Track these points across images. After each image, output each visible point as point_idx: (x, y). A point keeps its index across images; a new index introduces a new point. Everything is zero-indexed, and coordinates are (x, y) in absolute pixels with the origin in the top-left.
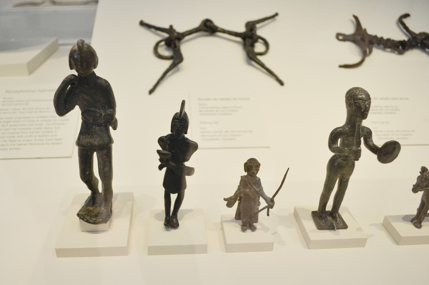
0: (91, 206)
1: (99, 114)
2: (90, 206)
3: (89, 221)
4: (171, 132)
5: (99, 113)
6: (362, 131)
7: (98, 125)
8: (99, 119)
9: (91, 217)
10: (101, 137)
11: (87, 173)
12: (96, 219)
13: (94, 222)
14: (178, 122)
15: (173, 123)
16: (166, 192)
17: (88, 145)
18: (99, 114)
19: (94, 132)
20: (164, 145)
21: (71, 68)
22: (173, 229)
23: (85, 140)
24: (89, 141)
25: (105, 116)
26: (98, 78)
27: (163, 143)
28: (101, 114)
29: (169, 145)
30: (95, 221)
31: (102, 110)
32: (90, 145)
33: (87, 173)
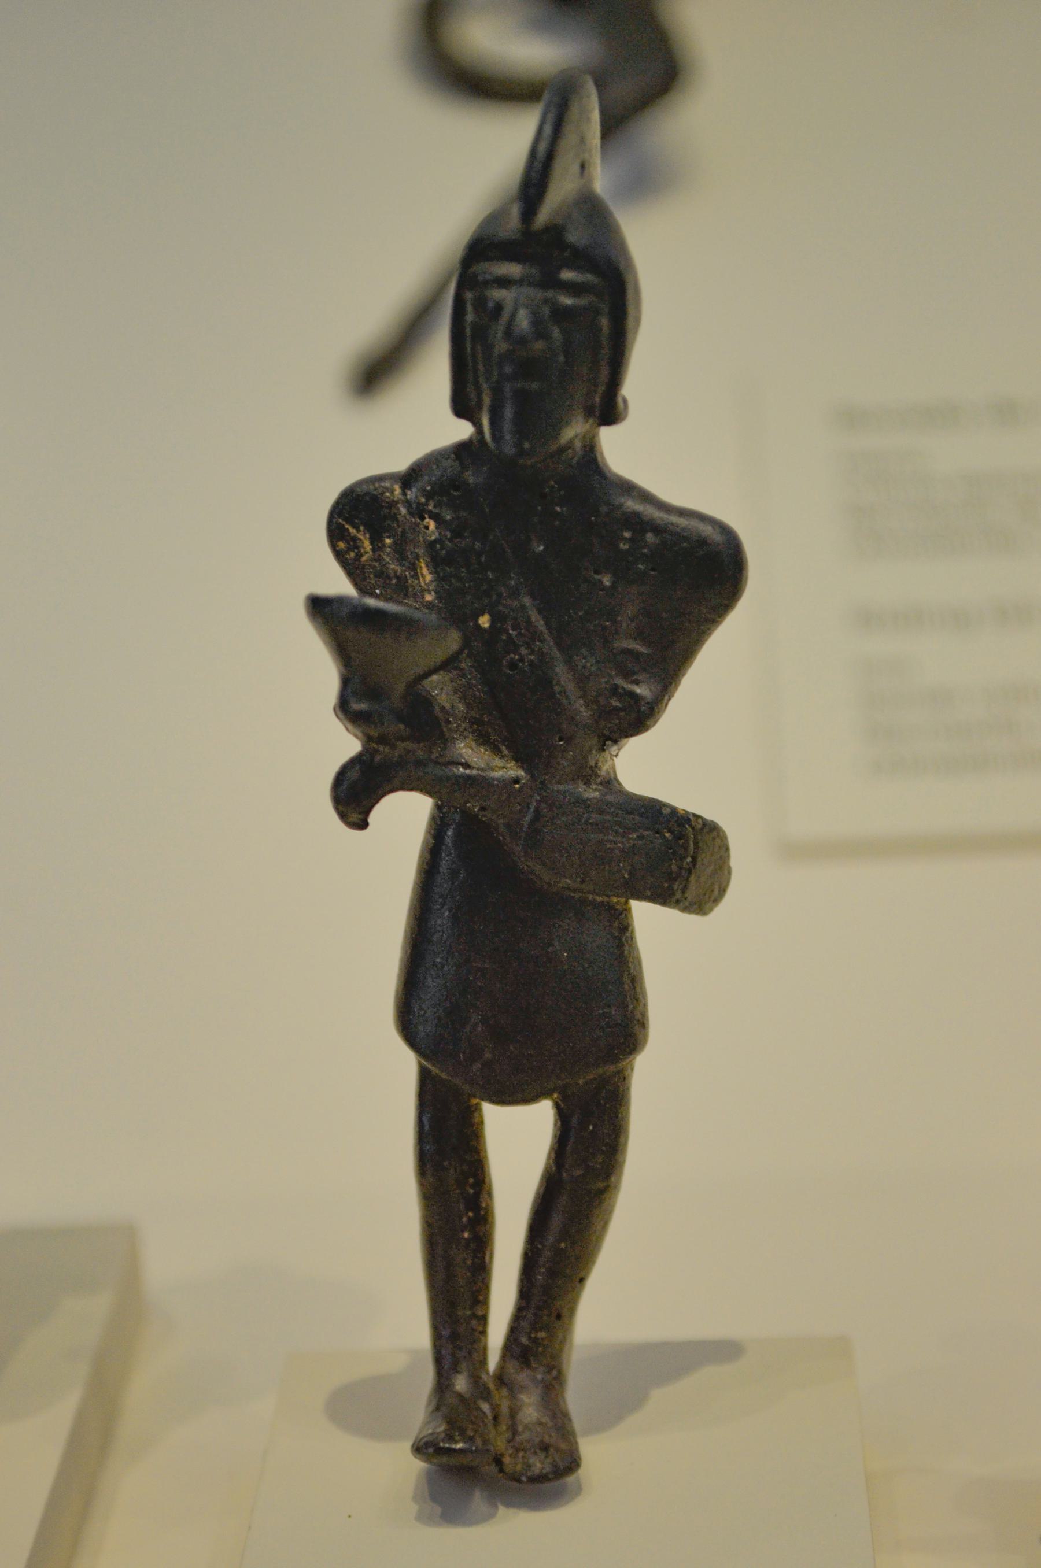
4: (462, 407)
14: (520, 282)
15: (469, 308)
16: (426, 1080)
20: (394, 567)
22: (509, 1505)
27: (376, 540)
29: (436, 563)
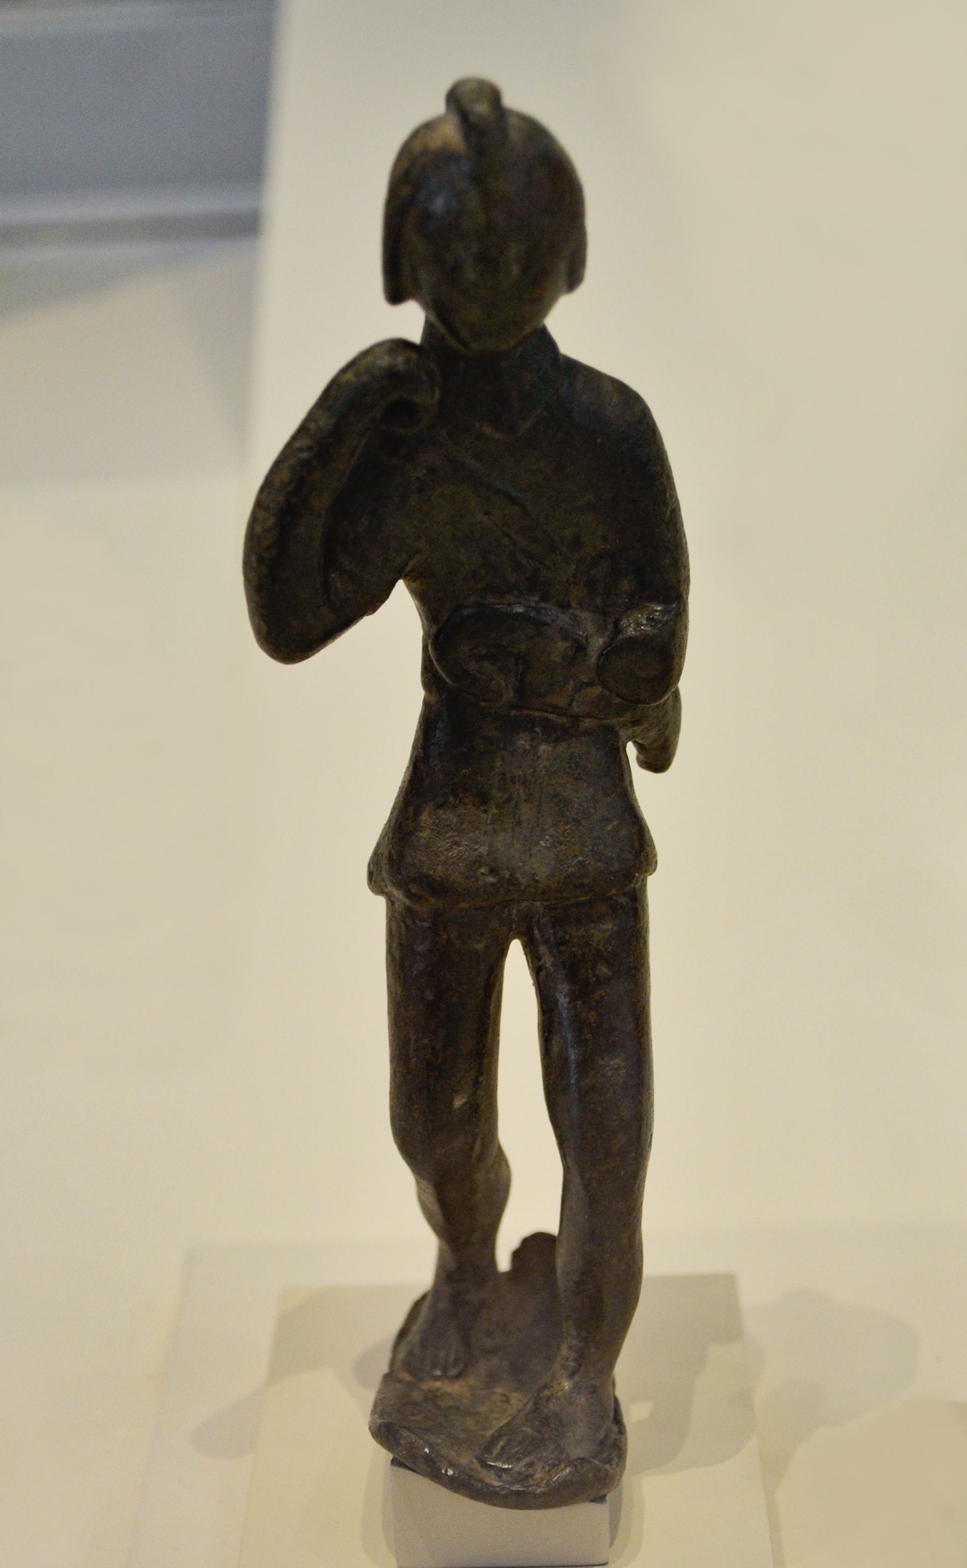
0: (453, 1372)
1: (562, 645)
2: (445, 1369)
3: (481, 1481)
5: (566, 638)
6: (410, 1039)
7: (548, 726)
8: (566, 682)
9: (488, 1448)
10: (577, 822)
11: (458, 1102)
12: (531, 1464)
13: (516, 1487)
17: (480, 883)
18: (562, 645)
19: (525, 783)
21: (395, 295)
23: (457, 844)
24: (490, 853)
25: (607, 654)
26: (573, 368)
28: (580, 648)
30: (523, 1478)
31: (584, 615)
32: (491, 879)
33: (458, 1102)
